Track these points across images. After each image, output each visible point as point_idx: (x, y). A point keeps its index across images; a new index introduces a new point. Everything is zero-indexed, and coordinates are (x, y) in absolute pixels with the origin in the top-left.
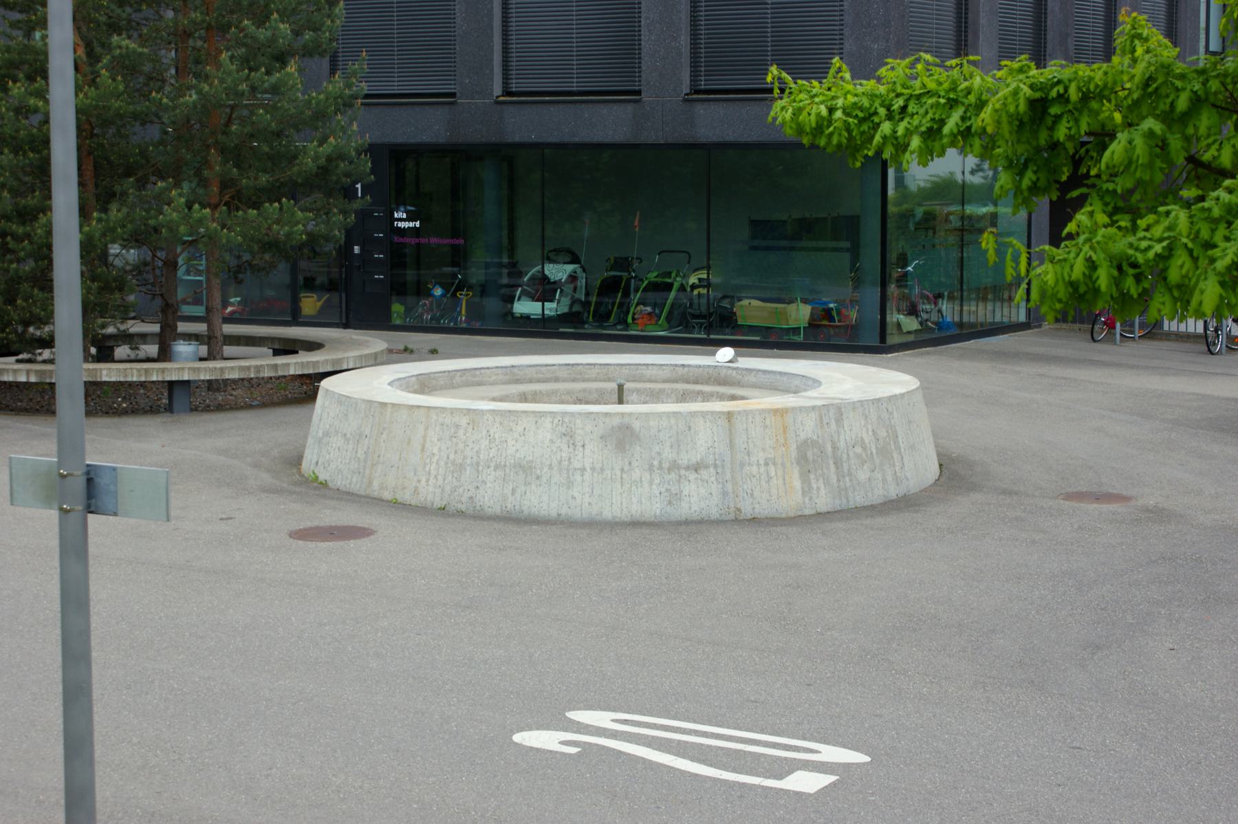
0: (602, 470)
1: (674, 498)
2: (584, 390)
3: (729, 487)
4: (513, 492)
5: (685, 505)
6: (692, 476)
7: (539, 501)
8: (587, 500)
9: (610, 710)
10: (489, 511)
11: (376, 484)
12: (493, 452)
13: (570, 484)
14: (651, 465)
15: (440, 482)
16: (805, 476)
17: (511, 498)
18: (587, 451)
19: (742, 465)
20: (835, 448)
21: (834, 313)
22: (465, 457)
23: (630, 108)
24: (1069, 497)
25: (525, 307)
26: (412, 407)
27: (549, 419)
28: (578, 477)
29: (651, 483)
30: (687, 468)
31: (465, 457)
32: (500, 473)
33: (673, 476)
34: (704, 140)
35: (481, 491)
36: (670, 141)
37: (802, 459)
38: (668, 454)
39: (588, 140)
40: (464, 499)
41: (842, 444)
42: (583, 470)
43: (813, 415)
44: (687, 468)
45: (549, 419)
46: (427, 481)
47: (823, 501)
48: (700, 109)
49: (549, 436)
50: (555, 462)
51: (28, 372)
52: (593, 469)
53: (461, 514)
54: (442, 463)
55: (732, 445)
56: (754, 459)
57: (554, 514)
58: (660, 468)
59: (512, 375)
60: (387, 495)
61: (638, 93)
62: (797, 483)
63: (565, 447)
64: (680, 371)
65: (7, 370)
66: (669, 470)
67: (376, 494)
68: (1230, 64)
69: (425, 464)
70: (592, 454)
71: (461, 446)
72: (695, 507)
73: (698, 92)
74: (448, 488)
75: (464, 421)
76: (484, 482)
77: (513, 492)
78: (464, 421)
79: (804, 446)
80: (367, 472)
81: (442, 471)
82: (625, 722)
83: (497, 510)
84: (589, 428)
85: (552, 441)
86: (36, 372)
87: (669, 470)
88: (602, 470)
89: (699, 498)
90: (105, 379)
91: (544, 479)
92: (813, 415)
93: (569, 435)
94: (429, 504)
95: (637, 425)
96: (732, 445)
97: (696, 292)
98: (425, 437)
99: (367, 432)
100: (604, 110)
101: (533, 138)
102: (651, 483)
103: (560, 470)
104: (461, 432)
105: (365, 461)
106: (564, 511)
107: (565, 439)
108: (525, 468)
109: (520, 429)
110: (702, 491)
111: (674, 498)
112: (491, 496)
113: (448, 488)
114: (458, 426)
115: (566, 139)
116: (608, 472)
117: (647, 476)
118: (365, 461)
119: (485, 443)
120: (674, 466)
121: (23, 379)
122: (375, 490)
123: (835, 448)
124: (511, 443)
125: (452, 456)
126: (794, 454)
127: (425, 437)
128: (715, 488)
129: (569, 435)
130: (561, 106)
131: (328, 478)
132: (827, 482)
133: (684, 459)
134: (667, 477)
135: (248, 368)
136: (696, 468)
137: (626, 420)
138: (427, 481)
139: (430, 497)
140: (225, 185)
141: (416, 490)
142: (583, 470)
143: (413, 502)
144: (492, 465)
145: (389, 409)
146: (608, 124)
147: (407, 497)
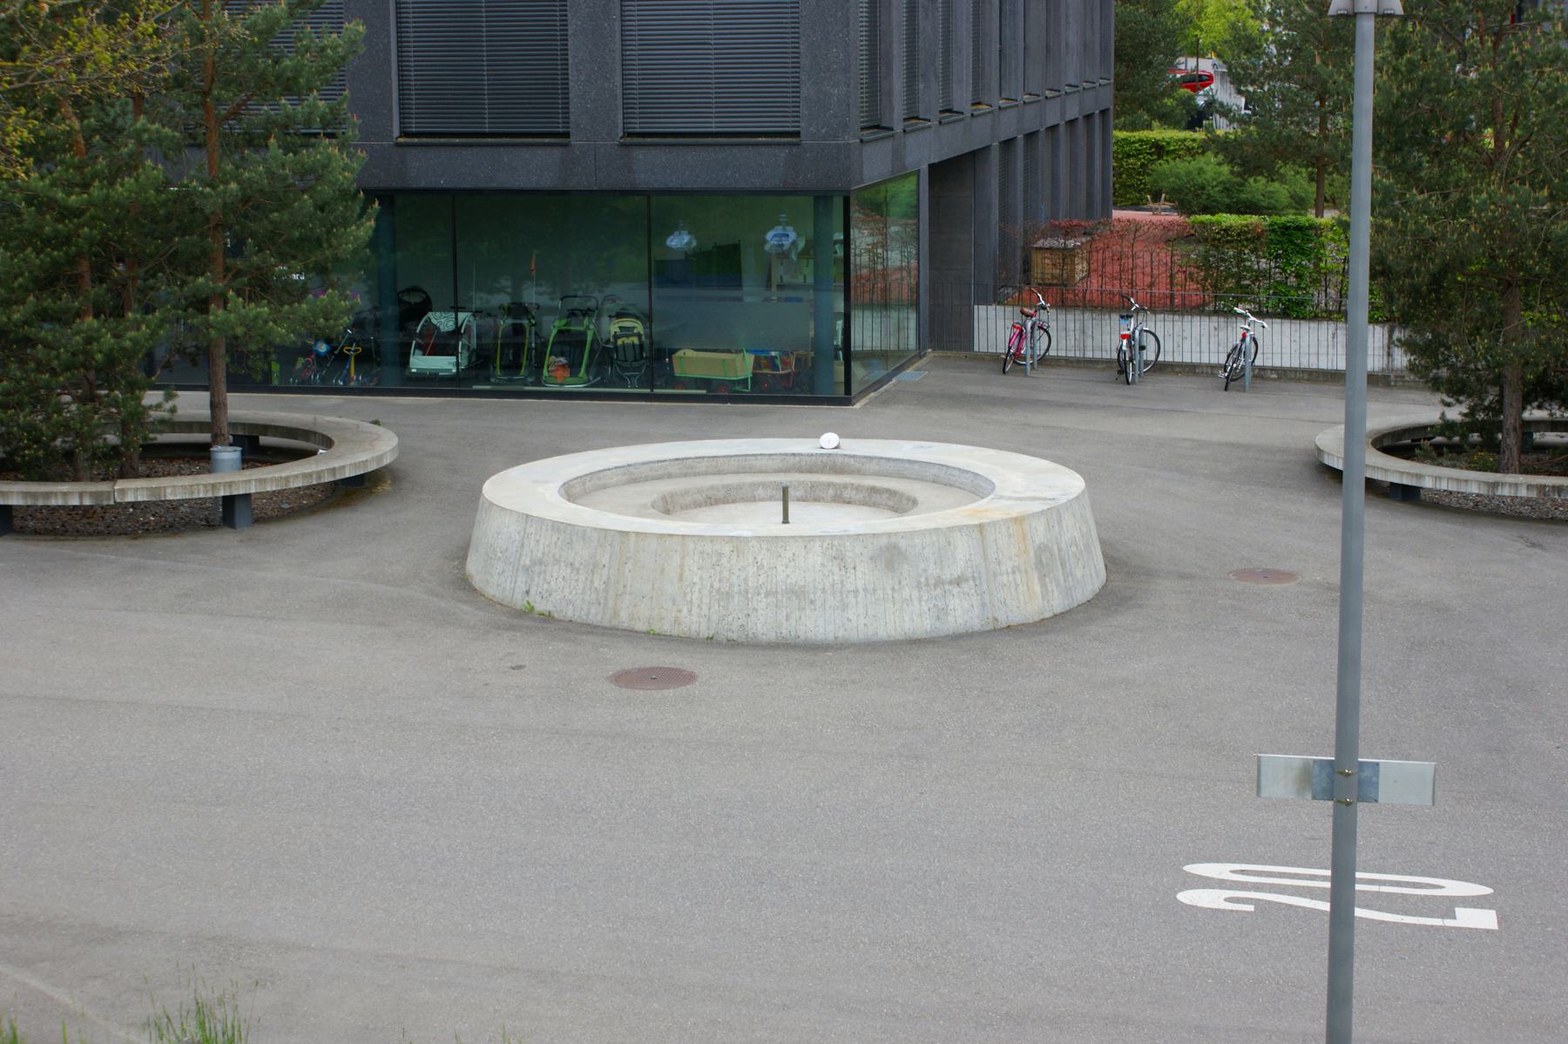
0: (875, 590)
1: (941, 613)
2: (712, 488)
3: (987, 598)
4: (788, 618)
5: (950, 619)
6: (955, 590)
7: (815, 625)
8: (862, 621)
9: (1229, 861)
10: (764, 639)
11: (624, 615)
12: (762, 579)
13: (844, 607)
14: (919, 583)
15: (705, 610)
16: (1042, 578)
17: (785, 624)
18: (859, 574)
19: (995, 575)
20: (1060, 550)
21: (778, 362)
22: (731, 585)
23: (557, 152)
24: (1246, 574)
25: (420, 362)
26: (662, 536)
27: (818, 543)
28: (852, 600)
29: (920, 600)
30: (951, 583)
31: (731, 585)
32: (771, 600)
33: (939, 591)
34: (643, 187)
35: (753, 618)
36: (605, 186)
37: (1039, 564)
38: (933, 570)
39: (507, 186)
40: (734, 627)
41: (1063, 546)
42: (856, 592)
43: (1043, 520)
44: (951, 583)
45: (818, 543)
46: (690, 611)
47: (1058, 604)
48: (639, 154)
49: (819, 560)
50: (828, 585)
51: (81, 495)
52: (865, 590)
53: (732, 644)
54: (706, 592)
55: (985, 556)
56: (1003, 568)
57: (830, 637)
58: (927, 585)
59: (633, 476)
60: (640, 626)
61: (567, 135)
62: (1037, 588)
63: (836, 570)
64: (792, 460)
65: (56, 494)
66: (936, 586)
67: (625, 625)
68: (1558, 229)
69: (685, 595)
70: (863, 576)
71: (726, 574)
72: (960, 621)
73: (630, 135)
74: (715, 618)
75: (727, 549)
76: (755, 610)
77: (788, 618)
78: (727, 549)
79: (1041, 549)
80: (611, 603)
81: (706, 600)
82: (1243, 872)
83: (772, 637)
84: (858, 550)
85: (823, 565)
86: (91, 494)
87: (936, 586)
88: (875, 590)
89: (962, 612)
90: (170, 497)
91: (818, 603)
92: (1043, 520)
93: (839, 558)
94: (693, 634)
95: (902, 544)
96: (985, 556)
97: (620, 342)
98: (681, 566)
99: (605, 561)
100: (525, 154)
101: (442, 183)
102: (920, 600)
103: (834, 594)
104: (724, 560)
105: (606, 591)
106: (841, 634)
107: (836, 562)
108: (798, 593)
109: (789, 554)
110: (965, 604)
111: (941, 613)
112: (764, 622)
113: (715, 618)
114: (720, 554)
115: (482, 185)
116: (880, 592)
117: (915, 593)
118: (606, 591)
119: (752, 570)
120: (939, 582)
121: (75, 502)
122: (624, 619)
123: (1060, 550)
124: (780, 568)
125: (716, 585)
126: (1033, 560)
127: (681, 566)
128: (975, 600)
129: (839, 558)
130: (475, 150)
131: (551, 608)
132: (1058, 585)
133: (947, 576)
134: (934, 593)
135: (310, 475)
136: (958, 582)
137: (893, 539)
138: (690, 611)
139: (694, 627)
140: (227, 269)
141: (677, 621)
142: (856, 592)
143: (675, 633)
144: (763, 591)
145: (633, 538)
146: (531, 168)
147: (666, 627)
